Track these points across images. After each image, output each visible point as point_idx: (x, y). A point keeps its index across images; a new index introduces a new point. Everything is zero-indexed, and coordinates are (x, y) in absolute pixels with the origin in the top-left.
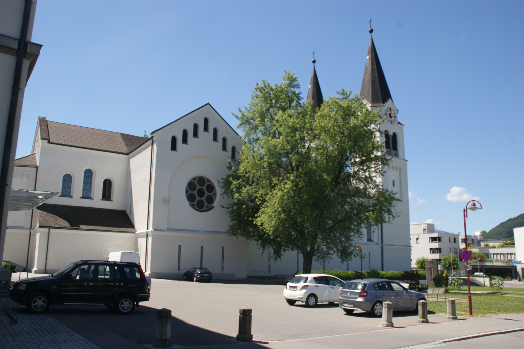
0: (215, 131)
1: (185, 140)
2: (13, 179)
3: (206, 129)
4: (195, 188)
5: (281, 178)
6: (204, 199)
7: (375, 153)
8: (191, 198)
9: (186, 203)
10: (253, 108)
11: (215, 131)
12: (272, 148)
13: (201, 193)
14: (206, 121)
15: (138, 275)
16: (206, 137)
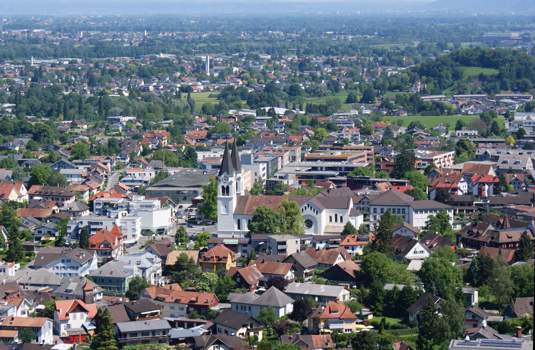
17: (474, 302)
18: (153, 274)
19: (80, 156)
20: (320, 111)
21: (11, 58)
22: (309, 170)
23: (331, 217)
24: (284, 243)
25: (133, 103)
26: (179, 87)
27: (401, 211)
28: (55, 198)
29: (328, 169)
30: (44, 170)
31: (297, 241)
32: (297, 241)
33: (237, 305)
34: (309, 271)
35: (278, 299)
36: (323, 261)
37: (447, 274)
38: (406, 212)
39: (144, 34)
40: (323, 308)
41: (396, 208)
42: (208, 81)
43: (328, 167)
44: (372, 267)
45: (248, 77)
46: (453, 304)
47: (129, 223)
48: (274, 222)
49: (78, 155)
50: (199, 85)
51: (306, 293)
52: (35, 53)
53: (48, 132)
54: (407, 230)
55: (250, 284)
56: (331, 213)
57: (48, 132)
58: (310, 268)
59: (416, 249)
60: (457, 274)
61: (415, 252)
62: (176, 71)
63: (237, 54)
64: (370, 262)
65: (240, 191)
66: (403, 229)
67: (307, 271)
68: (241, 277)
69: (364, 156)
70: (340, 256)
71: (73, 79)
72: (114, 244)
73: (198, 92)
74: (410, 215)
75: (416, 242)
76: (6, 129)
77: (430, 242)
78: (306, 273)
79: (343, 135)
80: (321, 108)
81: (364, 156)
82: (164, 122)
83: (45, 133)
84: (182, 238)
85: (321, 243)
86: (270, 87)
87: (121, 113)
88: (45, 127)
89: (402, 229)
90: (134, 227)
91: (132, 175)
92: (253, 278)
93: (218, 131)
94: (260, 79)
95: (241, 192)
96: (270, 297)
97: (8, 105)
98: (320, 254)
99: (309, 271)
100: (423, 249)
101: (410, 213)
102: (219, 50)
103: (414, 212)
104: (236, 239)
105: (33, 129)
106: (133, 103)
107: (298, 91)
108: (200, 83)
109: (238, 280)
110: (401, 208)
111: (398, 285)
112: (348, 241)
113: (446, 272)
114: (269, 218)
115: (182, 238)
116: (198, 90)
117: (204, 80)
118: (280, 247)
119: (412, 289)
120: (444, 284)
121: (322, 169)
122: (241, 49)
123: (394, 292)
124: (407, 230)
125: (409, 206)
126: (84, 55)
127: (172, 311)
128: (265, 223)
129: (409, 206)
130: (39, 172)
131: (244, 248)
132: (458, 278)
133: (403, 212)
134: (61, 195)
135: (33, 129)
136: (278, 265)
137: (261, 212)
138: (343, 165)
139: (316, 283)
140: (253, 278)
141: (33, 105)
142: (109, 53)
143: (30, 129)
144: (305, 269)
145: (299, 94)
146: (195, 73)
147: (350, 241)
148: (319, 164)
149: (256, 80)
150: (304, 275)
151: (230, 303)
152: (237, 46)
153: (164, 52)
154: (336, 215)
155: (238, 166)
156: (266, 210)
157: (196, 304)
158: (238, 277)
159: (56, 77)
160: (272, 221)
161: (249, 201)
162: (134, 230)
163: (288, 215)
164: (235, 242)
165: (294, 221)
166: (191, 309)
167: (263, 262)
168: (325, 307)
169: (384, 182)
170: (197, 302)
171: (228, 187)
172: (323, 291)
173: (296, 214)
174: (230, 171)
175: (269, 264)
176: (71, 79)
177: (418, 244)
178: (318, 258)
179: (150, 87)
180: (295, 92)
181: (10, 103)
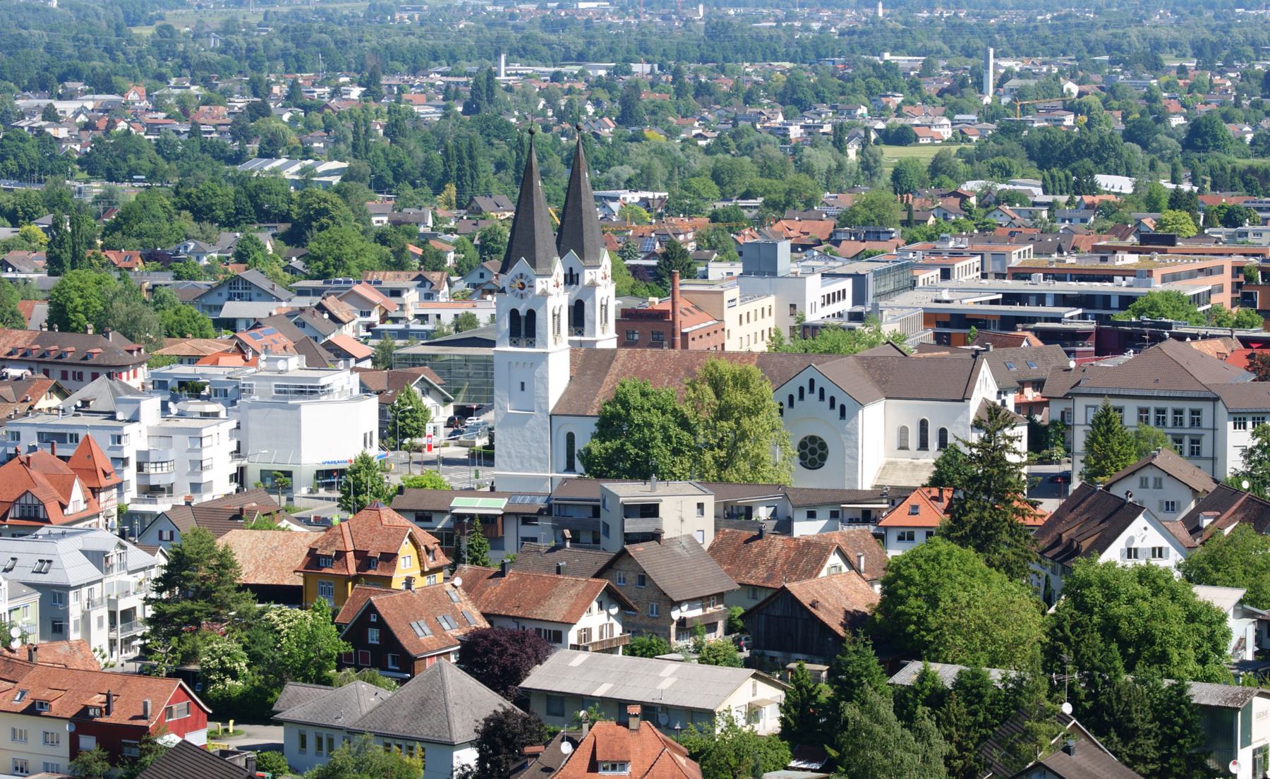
17: (1247, 742)
18: (104, 612)
19: (331, 270)
20: (1246, 184)
23: (904, 431)
24: (650, 511)
26: (878, 131)
27: (1169, 417)
28: (70, 370)
30: (92, 289)
31: (700, 506)
32: (700, 506)
33: (301, 730)
34: (698, 612)
35: (454, 711)
36: (770, 577)
37: (1158, 627)
38: (1206, 420)
39: (876, 13)
40: (566, 748)
41: (1170, 406)
42: (973, 117)
43: (1024, 279)
44: (912, 601)
46: (878, 728)
47: (181, 441)
49: (326, 266)
51: (599, 692)
53: (332, 218)
54: (1166, 482)
55: (413, 653)
56: (907, 413)
57: (332, 218)
58: (692, 602)
59: (1132, 539)
60: (1205, 630)
61: (1131, 553)
62: (895, 90)
63: (1106, 58)
64: (909, 581)
65: (593, 333)
66: (1149, 474)
67: (685, 612)
68: (382, 625)
69: (1221, 270)
70: (834, 559)
71: (590, 109)
72: (63, 507)
73: (932, 144)
74: (1218, 434)
75: (1135, 510)
76: (210, 208)
77: (1216, 518)
78: (682, 623)
79: (1246, 234)
80: (1249, 176)
81: (1221, 270)
83: (324, 220)
84: (361, 498)
85: (811, 516)
86: (1140, 128)
89: (1143, 473)
90: (196, 457)
91: (432, 319)
92: (437, 629)
93: (859, 219)
94: (1129, 113)
96: (423, 702)
97: (336, 165)
98: (762, 553)
99: (698, 612)
100: (1161, 542)
101: (1218, 426)
102: (1062, 46)
103: (1230, 424)
104: (502, 495)
105: (294, 207)
107: (1215, 138)
108: (945, 121)
109: (373, 636)
110: (1187, 406)
111: (935, 667)
112: (914, 510)
113: (1153, 617)
115: (361, 498)
116: (933, 139)
117: (962, 112)
118: (635, 525)
119: (989, 685)
120: (1119, 664)
121: (1041, 299)
122: (1126, 47)
123: (917, 693)
124: (1166, 482)
125: (1215, 399)
127: (18, 746)
128: (635, 445)
129: (1215, 399)
130: (74, 295)
131: (527, 531)
132: (1207, 646)
133: (1196, 422)
134: (90, 361)
135: (294, 207)
136: (555, 584)
137: (625, 403)
139: (702, 661)
140: (437, 629)
142: (737, 51)
143: (285, 207)
144: (678, 604)
145: (1216, 147)
146: (947, 96)
148: (1039, 285)
149: (1118, 114)
150: (673, 628)
151: (279, 723)
152: (1114, 35)
153: (895, 50)
154: (923, 425)
157: (105, 719)
158: (374, 625)
159: (542, 102)
160: (659, 436)
162: (198, 466)
163: (723, 413)
164: (496, 505)
165: (744, 436)
166: (88, 742)
167: (501, 574)
168: (575, 745)
169: (1219, 336)
170: (108, 713)
171: (531, 314)
172: (665, 685)
173: (751, 412)
174: (540, 254)
175: (522, 579)
177: (1140, 521)
178: (756, 565)
180: (1204, 141)
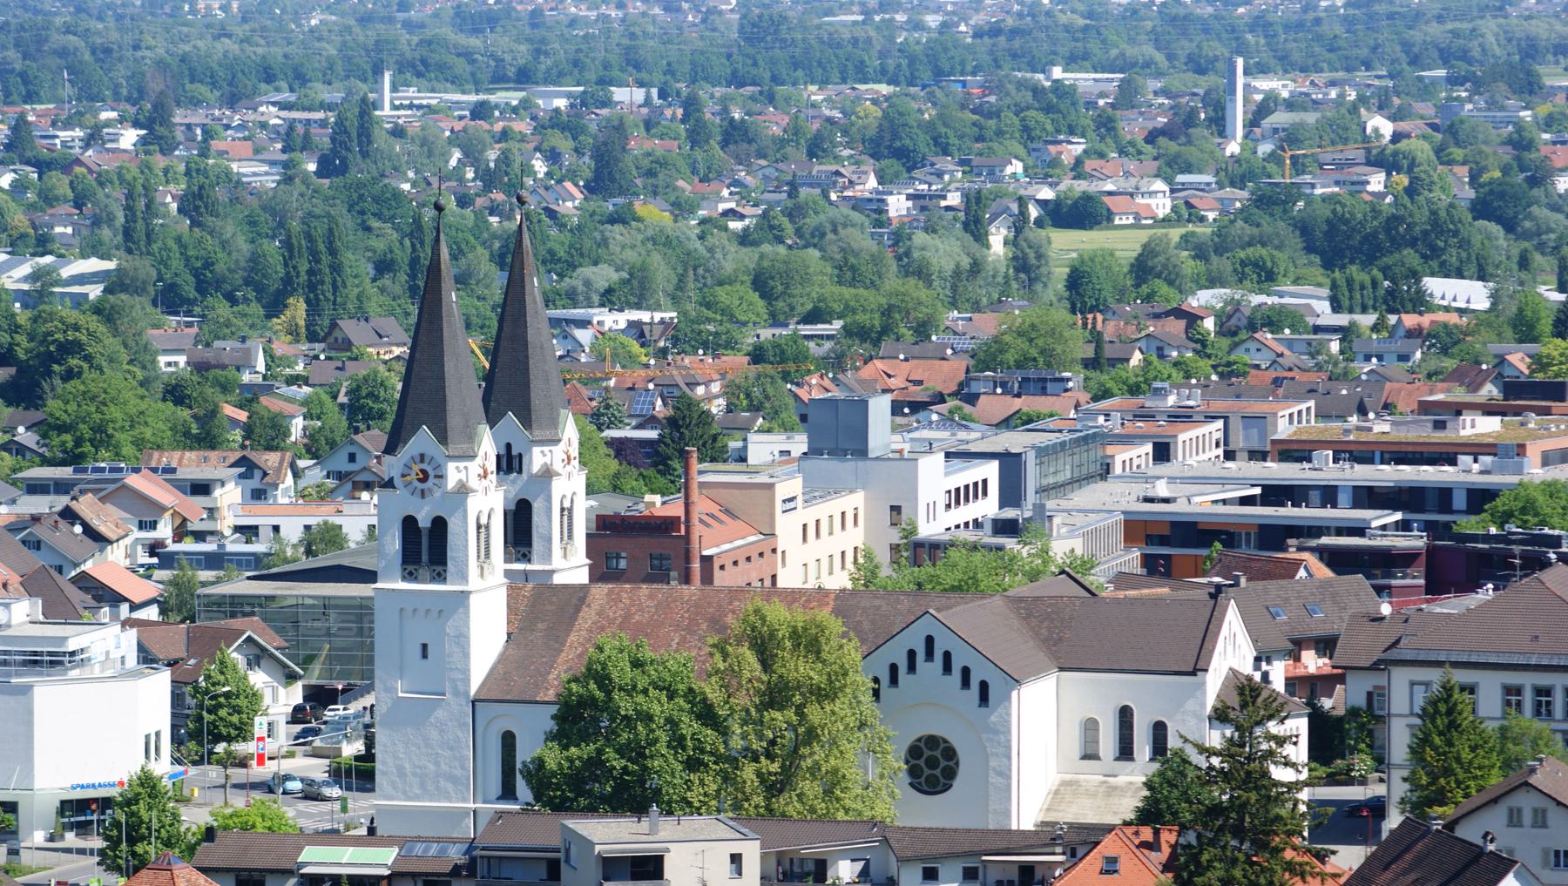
0: (966, 672)
1: (912, 668)
2: (1355, 868)
3: (930, 655)
4: (943, 770)
5: (1168, 817)
6: (937, 772)
7: (194, 431)
8: (951, 774)
9: (957, 783)
10: (1176, 793)
11: (947, 656)
12: (362, 426)
13: (932, 763)
14: (930, 641)
15: (1331, 810)
16: (930, 670)
19: (87, 448)
21: (299, 78)
22: (1246, 501)
23: (1090, 726)
25: (711, 250)
26: (1043, 203)
29: (1369, 497)
31: (736, 859)
32: (736, 859)
45: (1420, 157)
48: (678, 742)
49: (79, 442)
50: (1152, 194)
52: (424, 62)
56: (1096, 695)
62: (1072, 131)
82: (806, 330)
87: (609, 291)
88: (76, 328)
95: (557, 561)
102: (1364, 52)
105: (21, 339)
106: (711, 250)
114: (648, 718)
116: (1137, 217)
117: (1188, 169)
121: (1329, 495)
126: (670, 71)
128: (621, 752)
135: (21, 339)
138: (1463, 478)
141: (208, 265)
142: (796, 66)
147: (1125, 864)
148: (1326, 470)
149: (1463, 172)
152: (1456, 34)
154: (1125, 715)
155: (536, 401)
156: (637, 664)
159: (456, 156)
161: (587, 617)
163: (775, 696)
171: (440, 524)
173: (825, 694)
174: (454, 420)
176: (527, 170)
179: (891, 199)
181: (104, 256)
